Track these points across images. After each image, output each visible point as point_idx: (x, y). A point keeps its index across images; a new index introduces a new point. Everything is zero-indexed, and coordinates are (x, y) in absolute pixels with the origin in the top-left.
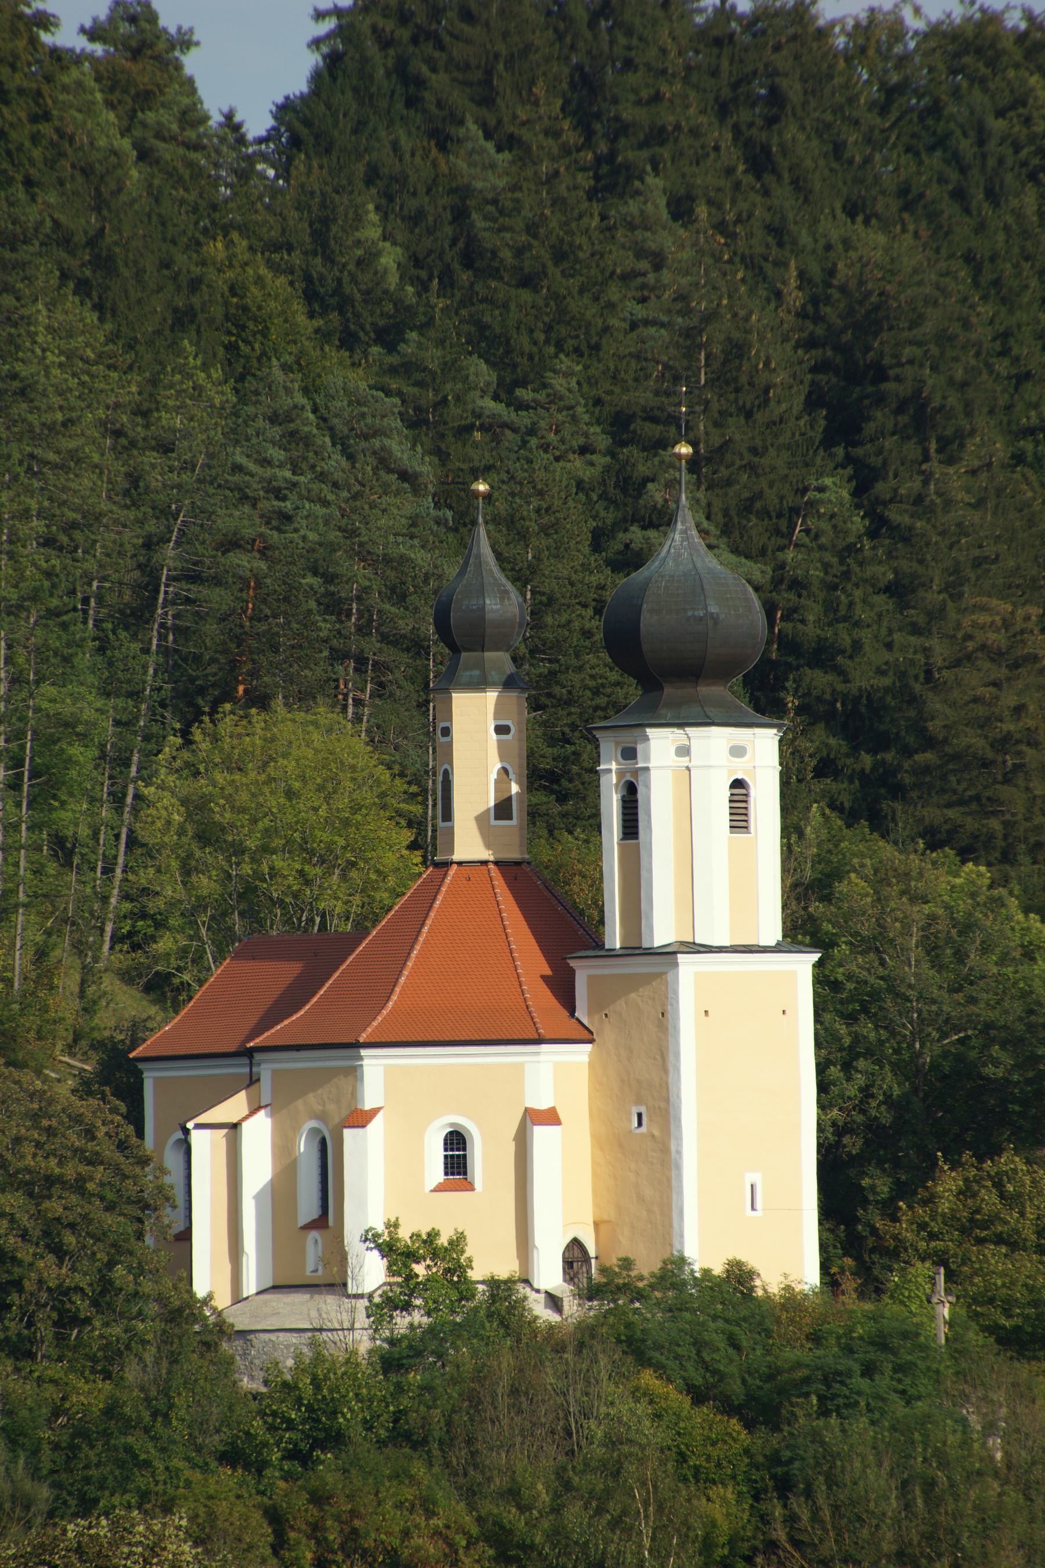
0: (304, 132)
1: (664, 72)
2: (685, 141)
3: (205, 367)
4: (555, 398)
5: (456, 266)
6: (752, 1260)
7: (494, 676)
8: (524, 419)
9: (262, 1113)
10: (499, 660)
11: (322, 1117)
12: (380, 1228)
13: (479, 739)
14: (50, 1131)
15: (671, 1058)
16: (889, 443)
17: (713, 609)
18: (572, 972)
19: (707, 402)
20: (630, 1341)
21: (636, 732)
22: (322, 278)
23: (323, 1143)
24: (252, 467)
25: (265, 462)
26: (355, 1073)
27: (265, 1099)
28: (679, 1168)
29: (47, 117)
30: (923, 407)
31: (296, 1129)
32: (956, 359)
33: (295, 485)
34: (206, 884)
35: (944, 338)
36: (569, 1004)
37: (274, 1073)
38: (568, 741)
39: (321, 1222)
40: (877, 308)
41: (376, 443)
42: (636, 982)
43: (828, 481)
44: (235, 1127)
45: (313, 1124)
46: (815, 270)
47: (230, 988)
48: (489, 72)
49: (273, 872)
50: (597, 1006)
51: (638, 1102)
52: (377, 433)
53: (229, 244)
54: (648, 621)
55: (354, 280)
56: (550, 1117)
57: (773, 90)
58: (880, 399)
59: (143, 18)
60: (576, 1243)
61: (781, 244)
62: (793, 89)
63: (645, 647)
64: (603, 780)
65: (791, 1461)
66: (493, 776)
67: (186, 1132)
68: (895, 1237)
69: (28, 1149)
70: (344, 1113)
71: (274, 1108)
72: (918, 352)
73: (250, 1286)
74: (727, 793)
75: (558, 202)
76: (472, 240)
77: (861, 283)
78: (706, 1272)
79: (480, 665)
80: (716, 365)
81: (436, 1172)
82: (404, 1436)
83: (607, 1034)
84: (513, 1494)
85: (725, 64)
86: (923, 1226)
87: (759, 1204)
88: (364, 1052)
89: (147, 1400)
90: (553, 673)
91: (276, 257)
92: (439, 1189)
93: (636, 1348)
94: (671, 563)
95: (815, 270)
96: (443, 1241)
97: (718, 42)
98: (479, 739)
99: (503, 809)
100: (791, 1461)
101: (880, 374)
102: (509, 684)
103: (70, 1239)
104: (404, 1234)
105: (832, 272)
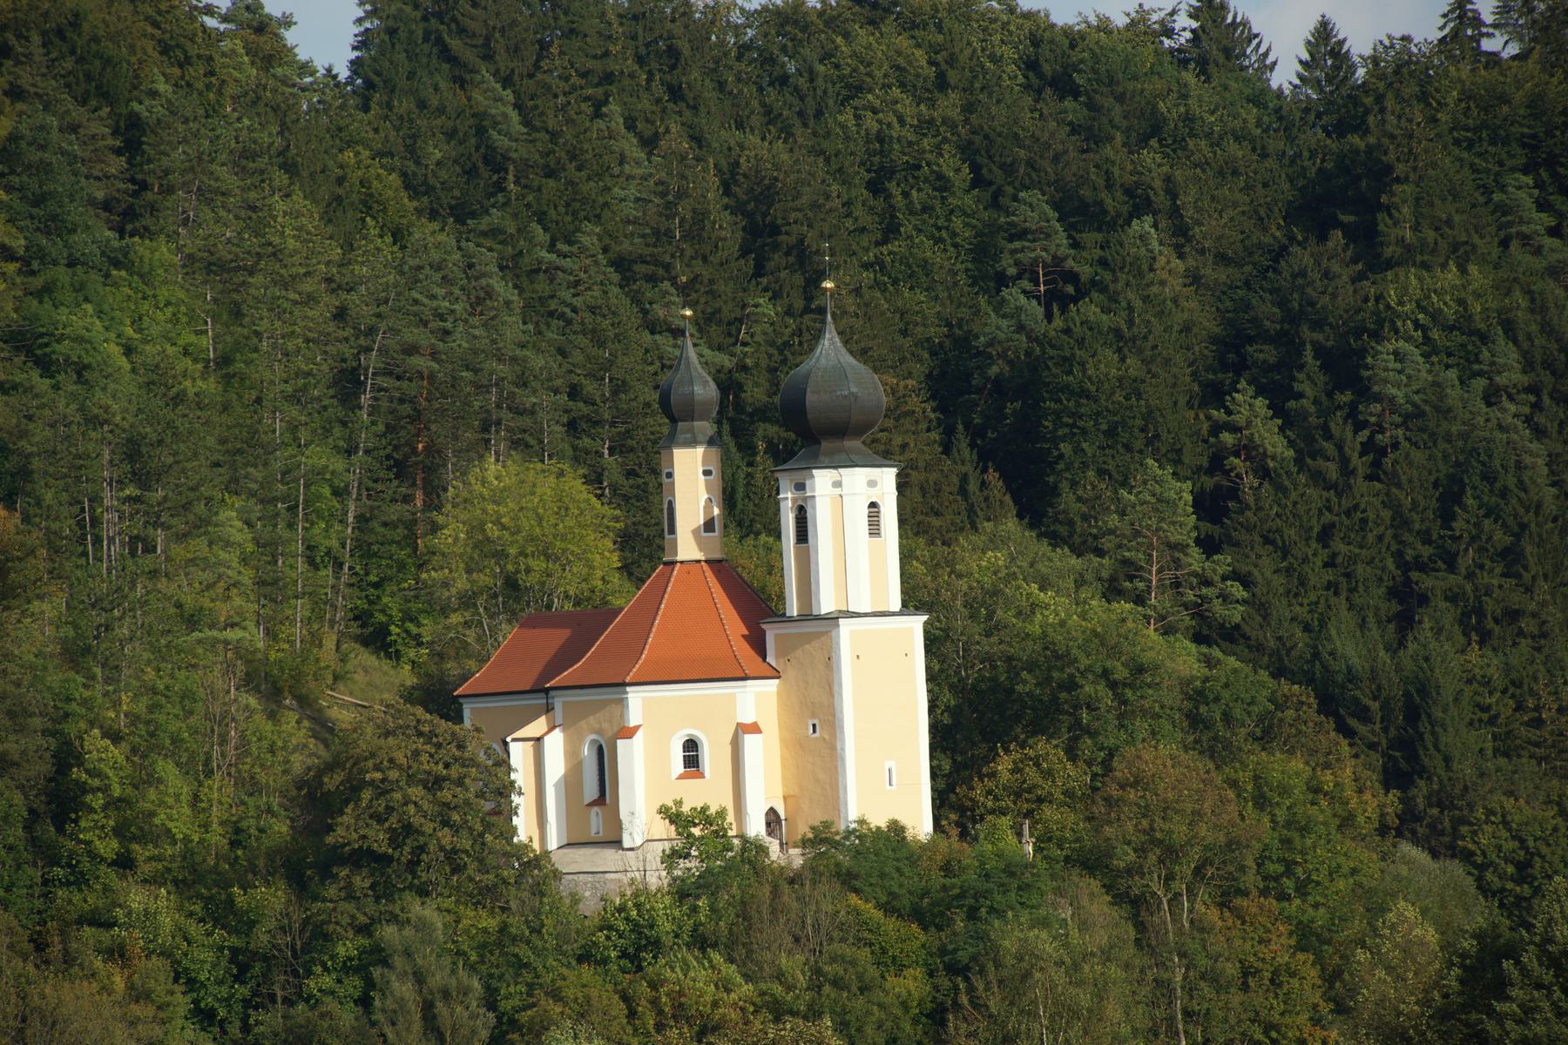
0: (376, 79)
1: (610, 37)
2: (626, 81)
3: (381, 236)
4: (583, 249)
5: (480, 164)
6: (905, 820)
7: (700, 437)
8: (567, 263)
9: (557, 730)
10: (706, 427)
11: (599, 732)
12: (670, 804)
13: (692, 480)
14: (439, 746)
15: (836, 687)
16: (783, 274)
17: (854, 390)
18: (763, 633)
19: (683, 250)
20: (838, 874)
21: (805, 472)
22: (414, 174)
23: (600, 749)
24: (426, 301)
25: (433, 297)
26: (622, 703)
27: (559, 720)
28: (843, 760)
29: (212, 73)
30: (804, 250)
31: (581, 740)
32: (824, 220)
33: (453, 311)
34: (483, 579)
35: (815, 206)
36: (762, 652)
37: (564, 703)
38: (637, 475)
39: (601, 800)
40: (768, 188)
41: (483, 282)
42: (810, 638)
43: (761, 301)
44: (539, 740)
45: (593, 737)
46: (723, 163)
47: (514, 647)
48: (488, 39)
49: (528, 571)
50: (781, 653)
51: (813, 716)
52: (484, 275)
53: (357, 154)
54: (811, 398)
55: (435, 175)
56: (754, 728)
57: (670, 48)
58: (776, 247)
59: (254, 8)
60: (772, 811)
61: (700, 147)
62: (684, 46)
63: (810, 417)
64: (782, 504)
65: (955, 951)
66: (702, 504)
67: (506, 744)
68: (972, 800)
69: (424, 758)
70: (616, 729)
71: (565, 727)
72: (800, 215)
73: (553, 844)
74: (866, 511)
75: (570, 121)
76: (491, 148)
77: (757, 172)
78: (878, 828)
79: (691, 430)
80: (687, 226)
81: (678, 766)
82: (701, 942)
83: (790, 673)
84: (779, 976)
85: (640, 32)
86: (989, 792)
87: (894, 781)
88: (628, 689)
89: (527, 922)
90: (628, 431)
91: (384, 161)
92: (681, 777)
93: (847, 880)
94: (823, 361)
95: (723, 163)
96: (712, 811)
97: (635, 18)
98: (692, 480)
99: (709, 525)
100: (955, 951)
101: (775, 230)
102: (710, 442)
103: (456, 817)
104: (686, 809)
105: (737, 164)
